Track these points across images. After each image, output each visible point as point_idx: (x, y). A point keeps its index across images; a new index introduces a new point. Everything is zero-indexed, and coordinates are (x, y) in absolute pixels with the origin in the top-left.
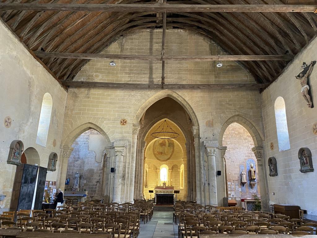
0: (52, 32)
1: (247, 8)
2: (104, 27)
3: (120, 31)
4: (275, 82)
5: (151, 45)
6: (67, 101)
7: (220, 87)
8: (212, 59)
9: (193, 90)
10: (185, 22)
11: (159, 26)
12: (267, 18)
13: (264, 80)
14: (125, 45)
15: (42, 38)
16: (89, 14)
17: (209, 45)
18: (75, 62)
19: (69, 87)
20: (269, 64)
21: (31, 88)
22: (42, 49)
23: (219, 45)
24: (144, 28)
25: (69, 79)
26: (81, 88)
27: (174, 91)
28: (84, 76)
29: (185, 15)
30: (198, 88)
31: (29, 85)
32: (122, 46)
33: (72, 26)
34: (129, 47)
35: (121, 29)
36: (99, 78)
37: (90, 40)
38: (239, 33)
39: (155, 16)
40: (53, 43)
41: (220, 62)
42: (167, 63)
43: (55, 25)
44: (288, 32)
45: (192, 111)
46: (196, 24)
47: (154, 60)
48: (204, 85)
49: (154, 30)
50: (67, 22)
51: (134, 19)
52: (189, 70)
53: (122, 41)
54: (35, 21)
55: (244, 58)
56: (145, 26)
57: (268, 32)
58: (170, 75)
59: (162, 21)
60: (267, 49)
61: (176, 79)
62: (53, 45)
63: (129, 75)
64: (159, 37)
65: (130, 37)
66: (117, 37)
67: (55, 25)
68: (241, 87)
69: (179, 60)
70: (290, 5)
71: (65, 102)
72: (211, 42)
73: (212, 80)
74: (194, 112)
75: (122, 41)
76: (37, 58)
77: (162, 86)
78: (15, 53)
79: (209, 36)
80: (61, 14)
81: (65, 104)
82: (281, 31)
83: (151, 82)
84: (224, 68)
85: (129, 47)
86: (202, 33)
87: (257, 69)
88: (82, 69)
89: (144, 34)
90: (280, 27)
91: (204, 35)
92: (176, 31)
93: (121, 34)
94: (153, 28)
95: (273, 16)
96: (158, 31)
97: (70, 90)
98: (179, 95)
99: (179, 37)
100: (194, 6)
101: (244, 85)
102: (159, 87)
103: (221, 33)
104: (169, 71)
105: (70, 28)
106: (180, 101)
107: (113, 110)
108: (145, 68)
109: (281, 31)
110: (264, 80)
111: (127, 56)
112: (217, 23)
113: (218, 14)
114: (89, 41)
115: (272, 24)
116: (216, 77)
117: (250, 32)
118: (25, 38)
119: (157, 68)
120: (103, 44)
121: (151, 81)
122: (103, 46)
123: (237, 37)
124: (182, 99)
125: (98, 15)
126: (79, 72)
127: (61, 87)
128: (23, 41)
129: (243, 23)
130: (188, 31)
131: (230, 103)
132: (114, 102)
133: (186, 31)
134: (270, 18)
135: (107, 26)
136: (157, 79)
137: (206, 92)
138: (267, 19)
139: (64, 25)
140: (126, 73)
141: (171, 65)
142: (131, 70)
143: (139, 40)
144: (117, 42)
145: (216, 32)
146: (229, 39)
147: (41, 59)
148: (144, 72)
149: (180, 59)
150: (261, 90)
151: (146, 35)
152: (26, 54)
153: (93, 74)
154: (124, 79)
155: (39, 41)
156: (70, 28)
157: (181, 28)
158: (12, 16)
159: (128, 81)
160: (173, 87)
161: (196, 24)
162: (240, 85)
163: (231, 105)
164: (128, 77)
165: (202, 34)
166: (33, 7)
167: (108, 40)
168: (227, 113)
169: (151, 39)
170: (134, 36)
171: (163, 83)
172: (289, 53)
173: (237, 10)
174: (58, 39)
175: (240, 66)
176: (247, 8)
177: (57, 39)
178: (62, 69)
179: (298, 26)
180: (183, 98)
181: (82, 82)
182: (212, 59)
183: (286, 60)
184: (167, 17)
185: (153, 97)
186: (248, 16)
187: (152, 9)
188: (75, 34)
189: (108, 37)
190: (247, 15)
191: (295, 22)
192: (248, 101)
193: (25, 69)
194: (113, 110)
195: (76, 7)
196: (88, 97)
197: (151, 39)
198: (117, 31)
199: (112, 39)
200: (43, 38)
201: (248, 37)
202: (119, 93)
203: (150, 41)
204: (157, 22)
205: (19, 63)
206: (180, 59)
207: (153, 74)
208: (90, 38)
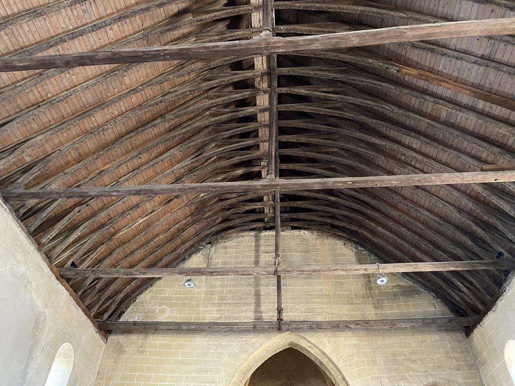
0: (95, 237)
1: (416, 178)
2: (183, 230)
3: (207, 236)
4: (491, 312)
5: (257, 256)
6: (102, 360)
7: (387, 324)
8: (366, 270)
9: (338, 333)
10: (310, 219)
11: (269, 226)
12: (447, 203)
13: (469, 311)
14: (214, 258)
15: (77, 247)
16: (159, 210)
17: (354, 254)
18: (128, 287)
19: (110, 334)
20: (472, 280)
21: (37, 333)
22: (73, 264)
23: (372, 253)
24: (245, 230)
25: (114, 317)
26: (132, 335)
27: (301, 335)
28: (139, 313)
29: (309, 207)
30: (347, 327)
31: (34, 328)
32: (208, 258)
33: (129, 227)
34: (221, 261)
35: (208, 232)
36: (165, 315)
37: (156, 251)
38: (403, 230)
39: (261, 199)
40: (93, 255)
41: (382, 275)
42: (286, 285)
43: (102, 226)
44: (493, 220)
45: (340, 377)
46: (329, 221)
47: (262, 275)
48: (357, 323)
49: (260, 232)
50: (122, 222)
51: (230, 218)
52: (326, 296)
53: (210, 252)
54: (69, 219)
55: (426, 267)
56: (247, 227)
57: (454, 225)
58: (291, 305)
59: (274, 219)
60: (459, 252)
61: (302, 312)
62: (93, 258)
63: (218, 307)
64: (270, 244)
65: (223, 244)
66: (202, 245)
67: (102, 226)
68: (427, 324)
69: (307, 273)
70: (489, 172)
71: (99, 362)
72: (357, 249)
73: (370, 313)
74: (344, 379)
75: (210, 252)
76: (61, 280)
77: (280, 326)
78: (22, 269)
79: (354, 239)
80: (111, 211)
81: (97, 368)
82: (477, 220)
83: (258, 319)
84: (387, 292)
85: (221, 261)
86: (341, 234)
87: (450, 291)
88: (137, 300)
89: (245, 239)
90: (475, 214)
91: (344, 237)
92: (296, 232)
93: (208, 240)
94: (260, 230)
95: (457, 199)
96: (268, 235)
97: (113, 338)
98: (313, 344)
99: (299, 242)
100: (326, 180)
101: (434, 321)
102: (273, 328)
103: (372, 232)
104: (290, 299)
105: (125, 231)
106: (315, 355)
107: (186, 378)
108: (248, 294)
109: (477, 220)
110: (469, 311)
111: (215, 270)
112: (363, 217)
113: (364, 190)
114: (155, 252)
115: (459, 212)
116: (376, 308)
117: (423, 228)
118: (49, 247)
119: (268, 294)
120: (178, 257)
121: (258, 319)
122: (179, 260)
123: (401, 236)
124: (318, 352)
125: (173, 211)
126: (133, 305)
127: (96, 333)
128: (43, 251)
129: (409, 215)
130: (316, 233)
131: (413, 357)
132: (188, 360)
133: (313, 233)
134: (452, 202)
135: (186, 229)
136: (270, 315)
137: (361, 336)
138: (448, 205)
139: (116, 226)
140: (213, 303)
141: (293, 287)
142: (223, 299)
143: (237, 248)
144: (202, 254)
145: (363, 231)
146: (387, 240)
147: (68, 280)
148: (244, 301)
149: (308, 271)
150: (468, 331)
151: (248, 240)
152: (44, 270)
153: (156, 308)
154: (210, 315)
155: (70, 252)
156: (125, 231)
157: (305, 229)
158: (33, 212)
159: (218, 319)
160: (298, 327)
161: (329, 221)
162: (426, 321)
163: (414, 361)
164: (217, 310)
165: (340, 237)
166: (67, 193)
167: (186, 250)
168: (411, 380)
169: (257, 246)
170: (229, 243)
171: (280, 319)
172: (505, 257)
173: (398, 182)
174: (104, 249)
175: (416, 287)
176: (416, 178)
177: (102, 249)
178: (103, 300)
179: (509, 209)
180: (320, 350)
181: (135, 323)
182: (366, 270)
183: (503, 268)
184: (282, 200)
185: (262, 349)
186: (414, 202)
187: (258, 188)
188: (132, 241)
189: (187, 245)
190: (413, 201)
191: (501, 203)
192: (447, 353)
193: (35, 296)
194: (186, 378)
195: (134, 190)
196: (142, 351)
197: (257, 246)
198: (202, 236)
199: (193, 249)
200: (78, 246)
201: (420, 236)
202: (200, 341)
203: (256, 250)
204: (266, 220)
205: (26, 286)
206: (308, 271)
207: (262, 305)
208: (156, 248)
